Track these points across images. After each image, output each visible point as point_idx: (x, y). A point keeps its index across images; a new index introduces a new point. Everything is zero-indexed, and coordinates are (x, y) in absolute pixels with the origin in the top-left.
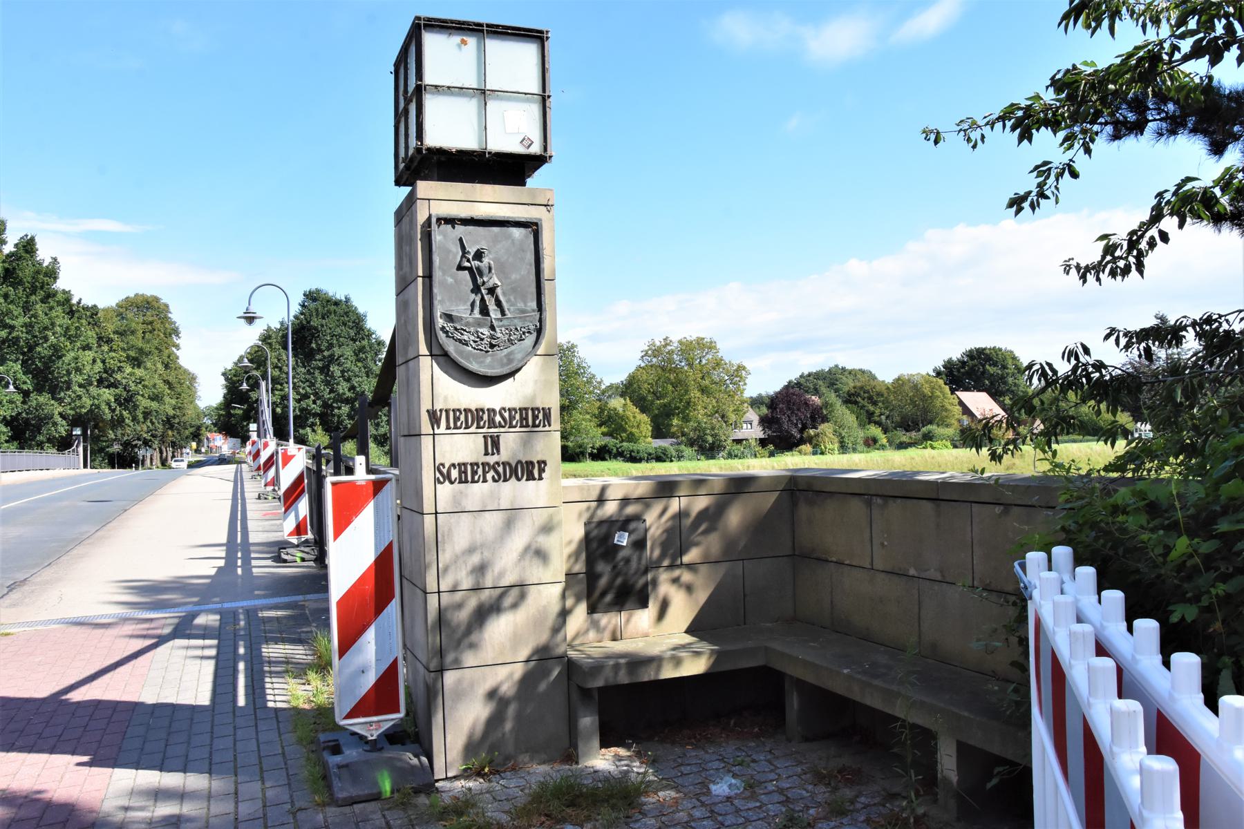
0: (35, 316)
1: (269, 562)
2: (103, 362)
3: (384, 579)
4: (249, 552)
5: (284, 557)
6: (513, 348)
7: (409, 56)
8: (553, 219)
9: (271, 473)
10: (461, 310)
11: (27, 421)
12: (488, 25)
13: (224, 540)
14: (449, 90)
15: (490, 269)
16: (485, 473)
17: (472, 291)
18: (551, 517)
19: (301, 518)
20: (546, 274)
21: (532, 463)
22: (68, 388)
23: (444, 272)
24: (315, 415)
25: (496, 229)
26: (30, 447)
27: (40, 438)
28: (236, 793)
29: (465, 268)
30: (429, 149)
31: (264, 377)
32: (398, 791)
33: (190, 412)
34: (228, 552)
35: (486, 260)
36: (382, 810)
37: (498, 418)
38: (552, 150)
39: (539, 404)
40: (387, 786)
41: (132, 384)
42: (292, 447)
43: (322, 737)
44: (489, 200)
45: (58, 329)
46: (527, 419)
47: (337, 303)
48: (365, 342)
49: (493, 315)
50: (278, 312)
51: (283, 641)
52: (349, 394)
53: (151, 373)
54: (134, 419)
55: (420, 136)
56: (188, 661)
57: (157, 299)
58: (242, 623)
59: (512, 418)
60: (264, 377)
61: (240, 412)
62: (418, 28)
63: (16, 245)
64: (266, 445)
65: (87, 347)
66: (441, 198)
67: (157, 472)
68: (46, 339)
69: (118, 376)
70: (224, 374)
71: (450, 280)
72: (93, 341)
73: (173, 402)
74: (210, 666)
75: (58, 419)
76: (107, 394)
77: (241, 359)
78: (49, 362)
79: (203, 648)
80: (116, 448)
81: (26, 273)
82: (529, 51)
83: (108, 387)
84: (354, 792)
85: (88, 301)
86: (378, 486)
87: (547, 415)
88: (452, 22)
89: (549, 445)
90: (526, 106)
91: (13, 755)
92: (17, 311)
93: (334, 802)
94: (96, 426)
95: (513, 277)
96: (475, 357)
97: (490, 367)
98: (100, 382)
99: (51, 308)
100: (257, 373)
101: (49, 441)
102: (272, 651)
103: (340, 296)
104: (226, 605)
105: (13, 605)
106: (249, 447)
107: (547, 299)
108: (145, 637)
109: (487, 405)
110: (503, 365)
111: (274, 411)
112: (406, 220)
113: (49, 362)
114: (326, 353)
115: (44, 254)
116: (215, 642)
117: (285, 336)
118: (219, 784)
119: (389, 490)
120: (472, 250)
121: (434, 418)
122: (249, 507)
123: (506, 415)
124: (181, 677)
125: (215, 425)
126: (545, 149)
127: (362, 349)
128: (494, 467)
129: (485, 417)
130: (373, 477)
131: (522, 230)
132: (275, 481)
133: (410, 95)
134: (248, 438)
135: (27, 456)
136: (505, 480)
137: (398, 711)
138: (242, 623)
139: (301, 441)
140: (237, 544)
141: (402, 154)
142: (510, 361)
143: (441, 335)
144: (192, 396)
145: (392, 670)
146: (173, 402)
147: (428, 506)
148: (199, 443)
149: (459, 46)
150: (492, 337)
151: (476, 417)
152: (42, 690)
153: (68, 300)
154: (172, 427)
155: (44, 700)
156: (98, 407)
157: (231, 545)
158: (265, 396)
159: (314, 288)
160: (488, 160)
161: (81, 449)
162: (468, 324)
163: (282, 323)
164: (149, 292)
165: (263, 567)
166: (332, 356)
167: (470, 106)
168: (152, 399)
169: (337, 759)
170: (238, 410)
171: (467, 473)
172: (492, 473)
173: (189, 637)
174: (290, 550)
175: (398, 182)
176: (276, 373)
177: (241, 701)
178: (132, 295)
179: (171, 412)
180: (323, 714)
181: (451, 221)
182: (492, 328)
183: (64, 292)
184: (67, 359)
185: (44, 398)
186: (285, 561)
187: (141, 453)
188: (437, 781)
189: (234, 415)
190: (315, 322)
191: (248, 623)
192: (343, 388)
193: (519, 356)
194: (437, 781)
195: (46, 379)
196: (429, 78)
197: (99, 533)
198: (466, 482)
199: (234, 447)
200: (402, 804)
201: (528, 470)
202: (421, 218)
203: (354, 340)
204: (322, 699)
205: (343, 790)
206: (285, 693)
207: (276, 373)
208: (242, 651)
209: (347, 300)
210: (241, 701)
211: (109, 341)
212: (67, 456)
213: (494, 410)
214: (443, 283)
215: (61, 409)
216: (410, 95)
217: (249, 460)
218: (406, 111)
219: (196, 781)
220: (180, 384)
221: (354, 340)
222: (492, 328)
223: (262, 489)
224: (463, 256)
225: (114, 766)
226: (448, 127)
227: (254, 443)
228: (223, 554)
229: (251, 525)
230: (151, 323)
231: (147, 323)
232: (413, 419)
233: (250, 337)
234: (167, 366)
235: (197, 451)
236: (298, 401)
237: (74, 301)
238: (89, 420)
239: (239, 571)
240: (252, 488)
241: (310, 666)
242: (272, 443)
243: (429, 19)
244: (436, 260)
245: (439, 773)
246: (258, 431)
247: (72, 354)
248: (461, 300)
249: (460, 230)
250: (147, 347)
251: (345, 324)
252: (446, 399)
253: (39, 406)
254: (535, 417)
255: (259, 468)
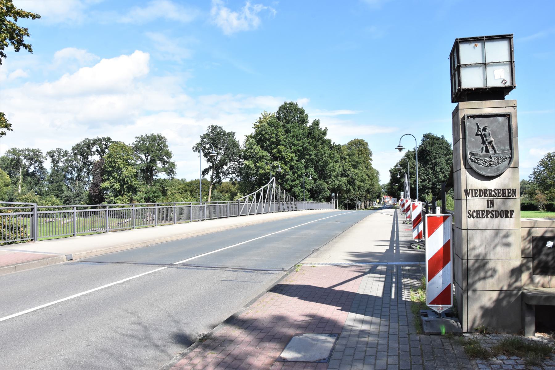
0: (319, 150)
1: (406, 249)
2: (343, 167)
3: (445, 254)
4: (399, 244)
5: (413, 247)
6: (499, 165)
7: (455, 54)
8: (516, 112)
9: (409, 213)
10: (478, 151)
11: (316, 190)
12: (486, 37)
13: (389, 239)
14: (471, 66)
15: (489, 134)
16: (487, 214)
17: (482, 143)
18: (507, 233)
19: (420, 231)
20: (513, 135)
21: (507, 211)
22: (330, 178)
23: (470, 136)
24: (429, 188)
25: (492, 118)
26: (317, 200)
27: (320, 197)
28: (389, 326)
29: (479, 135)
30: (463, 90)
31: (407, 172)
32: (448, 333)
33: (377, 187)
34: (390, 243)
35: (487, 131)
36: (441, 339)
37: (493, 193)
38: (516, 83)
39: (511, 187)
40: (444, 331)
41: (354, 176)
42: (417, 202)
43: (421, 311)
44: (489, 107)
45: (327, 155)
46: (505, 193)
47: (438, 139)
48: (451, 156)
49: (491, 153)
50: (412, 144)
51: (410, 278)
52: (443, 179)
53: (361, 171)
54: (354, 190)
55: (460, 85)
56: (375, 282)
57: (363, 141)
58: (395, 270)
59: (499, 193)
60: (407, 172)
61: (396, 187)
62: (458, 42)
63: (312, 123)
64: (407, 201)
65: (337, 161)
66: (470, 108)
67: (363, 211)
68: (322, 159)
69: (349, 173)
70: (390, 171)
71: (473, 140)
72: (339, 159)
73: (370, 183)
74: (382, 285)
75: (327, 190)
76: (344, 180)
77: (397, 165)
78: (323, 167)
79: (380, 278)
80: (348, 201)
81: (316, 134)
82: (504, 44)
83: (345, 177)
84: (431, 331)
85: (337, 143)
86: (445, 218)
87: (514, 192)
88: (471, 38)
89: (515, 203)
90: (503, 67)
91: (318, 304)
92: (312, 148)
93: (423, 333)
94: (340, 193)
95: (499, 137)
96: (483, 169)
97: (489, 173)
98: (342, 175)
99: (324, 147)
100: (404, 171)
101: (323, 198)
102: (406, 281)
103: (439, 136)
104: (389, 263)
105: (315, 257)
106: (400, 202)
107: (514, 145)
108: (359, 272)
109: (489, 188)
110: (495, 172)
111: (411, 187)
112: (456, 116)
113: (323, 167)
114: (433, 161)
115: (322, 127)
116: (384, 276)
117: (415, 154)
118: (383, 322)
119: (449, 220)
120: (482, 127)
121: (467, 193)
122: (399, 226)
123: (497, 192)
124: (372, 286)
125: (386, 192)
126: (512, 84)
127: (449, 159)
128: (491, 212)
129: (488, 192)
130: (443, 215)
131: (503, 118)
132: (410, 217)
133: (456, 69)
134: (400, 198)
135: (316, 204)
136: (496, 218)
137: (450, 304)
138: (395, 270)
139: (422, 199)
140: (394, 241)
141: (454, 92)
142: (498, 170)
143: (470, 161)
144: (377, 180)
145: (448, 288)
146: (370, 183)
147: (464, 227)
148: (380, 200)
149: (474, 47)
150: (490, 161)
151: (484, 192)
152: (326, 286)
153: (330, 143)
154: (369, 193)
155: (326, 289)
156: (341, 185)
157: (392, 241)
158: (407, 180)
159: (427, 133)
160: (488, 91)
161: (334, 202)
162: (480, 156)
163: (414, 149)
164: (360, 138)
165: (404, 250)
166: (436, 162)
167: (480, 70)
168: (361, 182)
169: (426, 318)
170: (396, 186)
171: (480, 214)
172: (490, 214)
173: (375, 273)
174: (415, 244)
175: (453, 102)
176: (412, 170)
177: (393, 297)
178: (353, 140)
179: (369, 187)
180: (422, 304)
181: (473, 117)
182: (491, 157)
183: (328, 140)
184: (330, 166)
185: (321, 182)
186: (413, 248)
187: (357, 203)
188: (464, 333)
189: (394, 188)
190: (428, 148)
191: (397, 270)
192: (441, 176)
193: (502, 168)
194: (464, 333)
195: (322, 174)
196: (463, 62)
197: (343, 234)
198: (480, 218)
199: (394, 202)
200: (449, 338)
201: (507, 214)
202: (461, 116)
203: (446, 155)
204: (422, 299)
205: (427, 330)
206: (408, 296)
207: (412, 170)
208: (394, 280)
209: (443, 137)
210: (393, 297)
211: (345, 158)
212: (329, 204)
213: (491, 190)
214: (470, 141)
215: (327, 186)
216: (456, 69)
217: (400, 207)
218: (455, 74)
219: (376, 320)
220: (373, 175)
221: (446, 155)
222: (491, 157)
223: (405, 219)
224: (478, 130)
225: (349, 311)
226: (471, 80)
227: (402, 200)
228: (389, 244)
229: (400, 234)
230: (361, 151)
231: (360, 149)
232: (459, 194)
233: (401, 155)
234: (367, 168)
235: (379, 203)
236: (421, 182)
237: (332, 143)
238: (338, 190)
239: (395, 251)
240: (401, 219)
241: (419, 288)
242: (409, 201)
243: (461, 39)
244: (467, 132)
245: (465, 329)
246: (404, 195)
247: (332, 164)
248: (477, 147)
249: (477, 120)
250: (359, 161)
251: (441, 148)
252: (471, 185)
253: (320, 184)
254: (509, 193)
255: (404, 211)
